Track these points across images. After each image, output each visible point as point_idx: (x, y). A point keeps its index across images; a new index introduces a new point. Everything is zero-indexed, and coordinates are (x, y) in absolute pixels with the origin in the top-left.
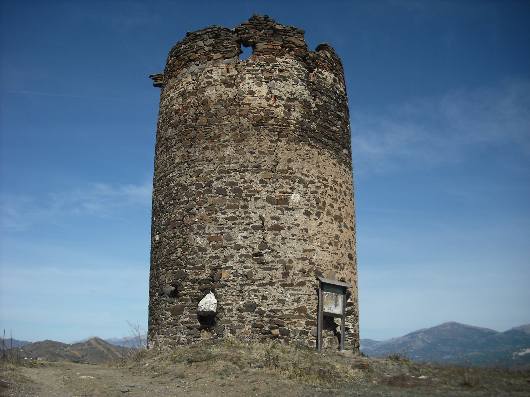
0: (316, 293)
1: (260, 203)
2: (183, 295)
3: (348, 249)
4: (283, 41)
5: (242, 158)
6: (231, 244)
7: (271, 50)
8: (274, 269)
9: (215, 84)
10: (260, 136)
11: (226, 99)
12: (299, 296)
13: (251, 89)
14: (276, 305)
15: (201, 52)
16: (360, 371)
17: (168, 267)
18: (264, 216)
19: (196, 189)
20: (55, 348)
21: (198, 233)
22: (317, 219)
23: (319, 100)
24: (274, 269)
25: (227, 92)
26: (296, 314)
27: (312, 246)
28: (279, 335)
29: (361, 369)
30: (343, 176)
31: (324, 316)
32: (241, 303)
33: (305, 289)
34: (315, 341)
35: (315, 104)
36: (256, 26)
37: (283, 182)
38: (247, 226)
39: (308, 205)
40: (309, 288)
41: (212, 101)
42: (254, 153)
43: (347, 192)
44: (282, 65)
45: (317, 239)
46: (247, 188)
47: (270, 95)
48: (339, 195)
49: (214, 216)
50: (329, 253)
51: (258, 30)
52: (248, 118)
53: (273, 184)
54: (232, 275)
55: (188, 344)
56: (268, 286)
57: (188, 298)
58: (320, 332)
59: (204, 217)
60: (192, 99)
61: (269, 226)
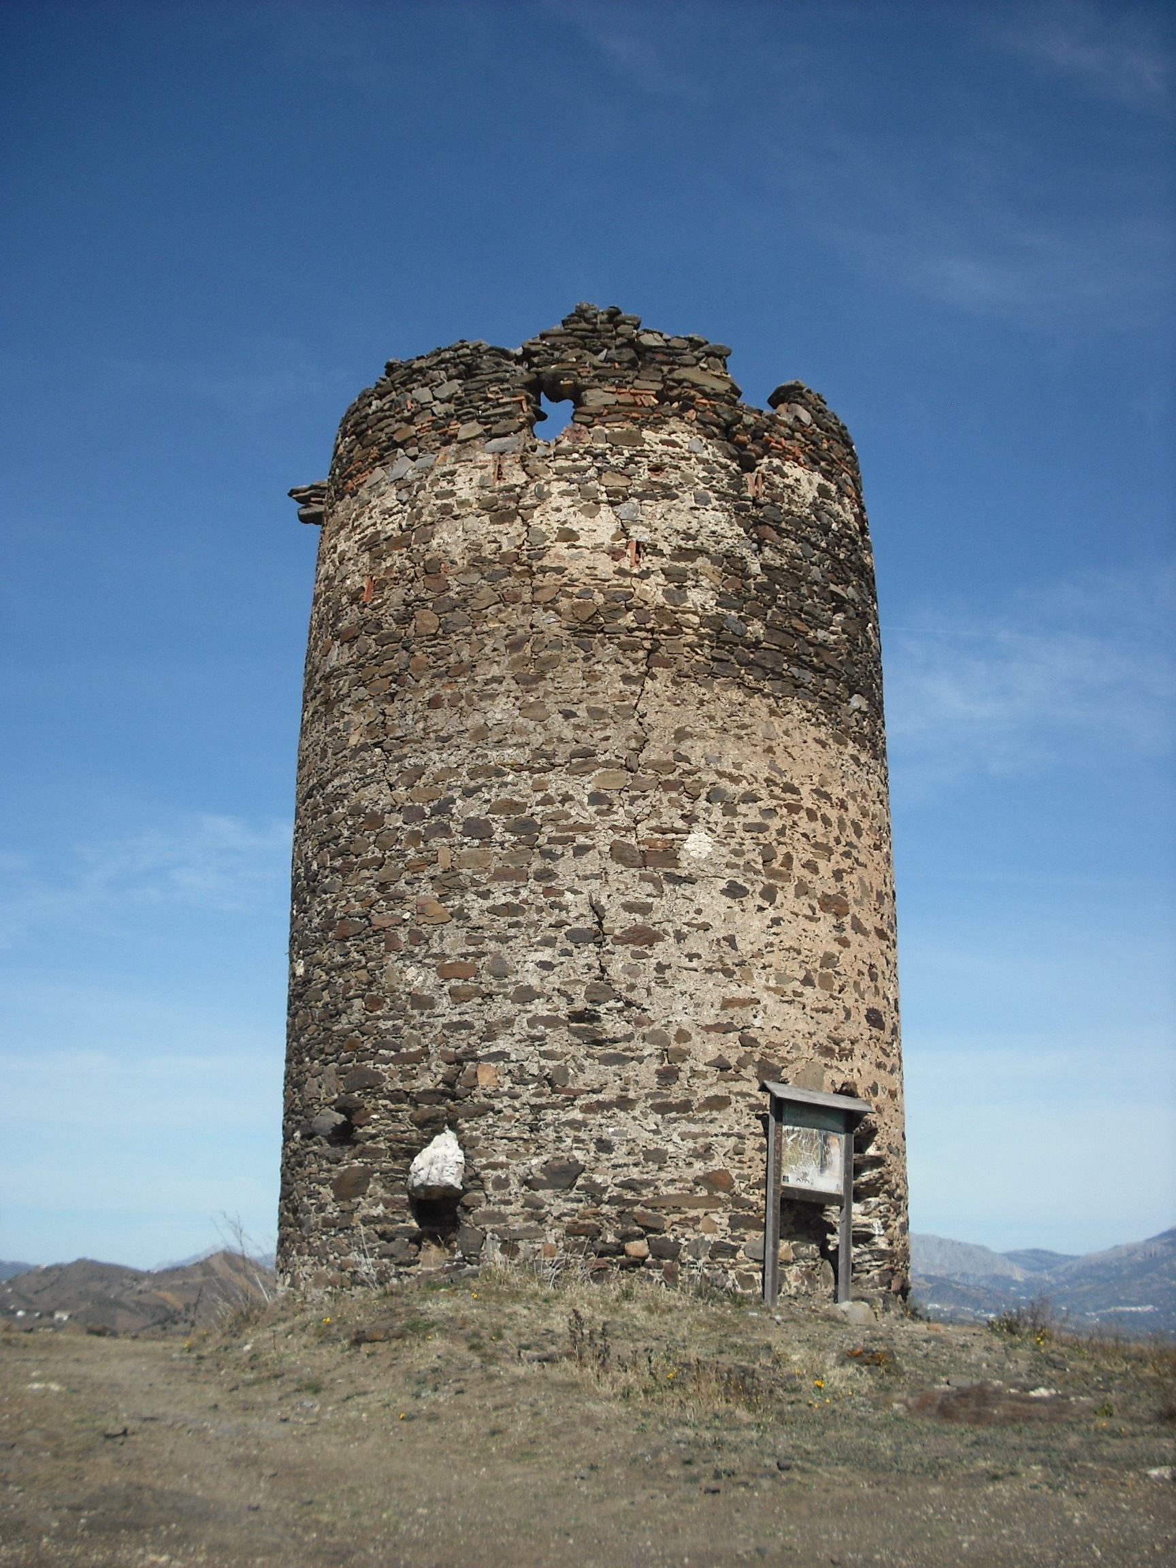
0: (761, 1130)
1: (590, 863)
2: (367, 1137)
3: (866, 996)
4: (663, 381)
5: (539, 729)
6: (505, 986)
7: (626, 409)
8: (633, 1059)
9: (463, 512)
10: (591, 662)
11: (491, 557)
12: (710, 1139)
13: (566, 526)
14: (640, 1168)
15: (423, 420)
16: (861, 1373)
17: (327, 1054)
18: (604, 901)
19: (405, 823)
20: (105, 1283)
21: (411, 955)
22: (764, 909)
23: (771, 553)
24: (633, 1059)
25: (496, 535)
26: (700, 1195)
27: (749, 989)
28: (647, 1257)
29: (868, 1364)
30: (850, 777)
31: (783, 1201)
32: (535, 1161)
33: (726, 1120)
34: (760, 1274)
35: (761, 564)
36: (582, 338)
37: (660, 800)
38: (551, 933)
39: (736, 866)
40: (739, 1115)
41: (453, 562)
42: (574, 715)
43: (865, 825)
44: (659, 453)
45: (764, 967)
46: (553, 820)
47: (624, 541)
48: (836, 832)
49: (456, 902)
50: (804, 1008)
51: (590, 350)
52: (558, 612)
53: (631, 805)
54: (508, 1078)
55: (381, 1284)
56: (616, 1110)
57: (382, 1146)
58: (771, 1247)
59: (429, 907)
60: (396, 557)
61: (617, 932)
